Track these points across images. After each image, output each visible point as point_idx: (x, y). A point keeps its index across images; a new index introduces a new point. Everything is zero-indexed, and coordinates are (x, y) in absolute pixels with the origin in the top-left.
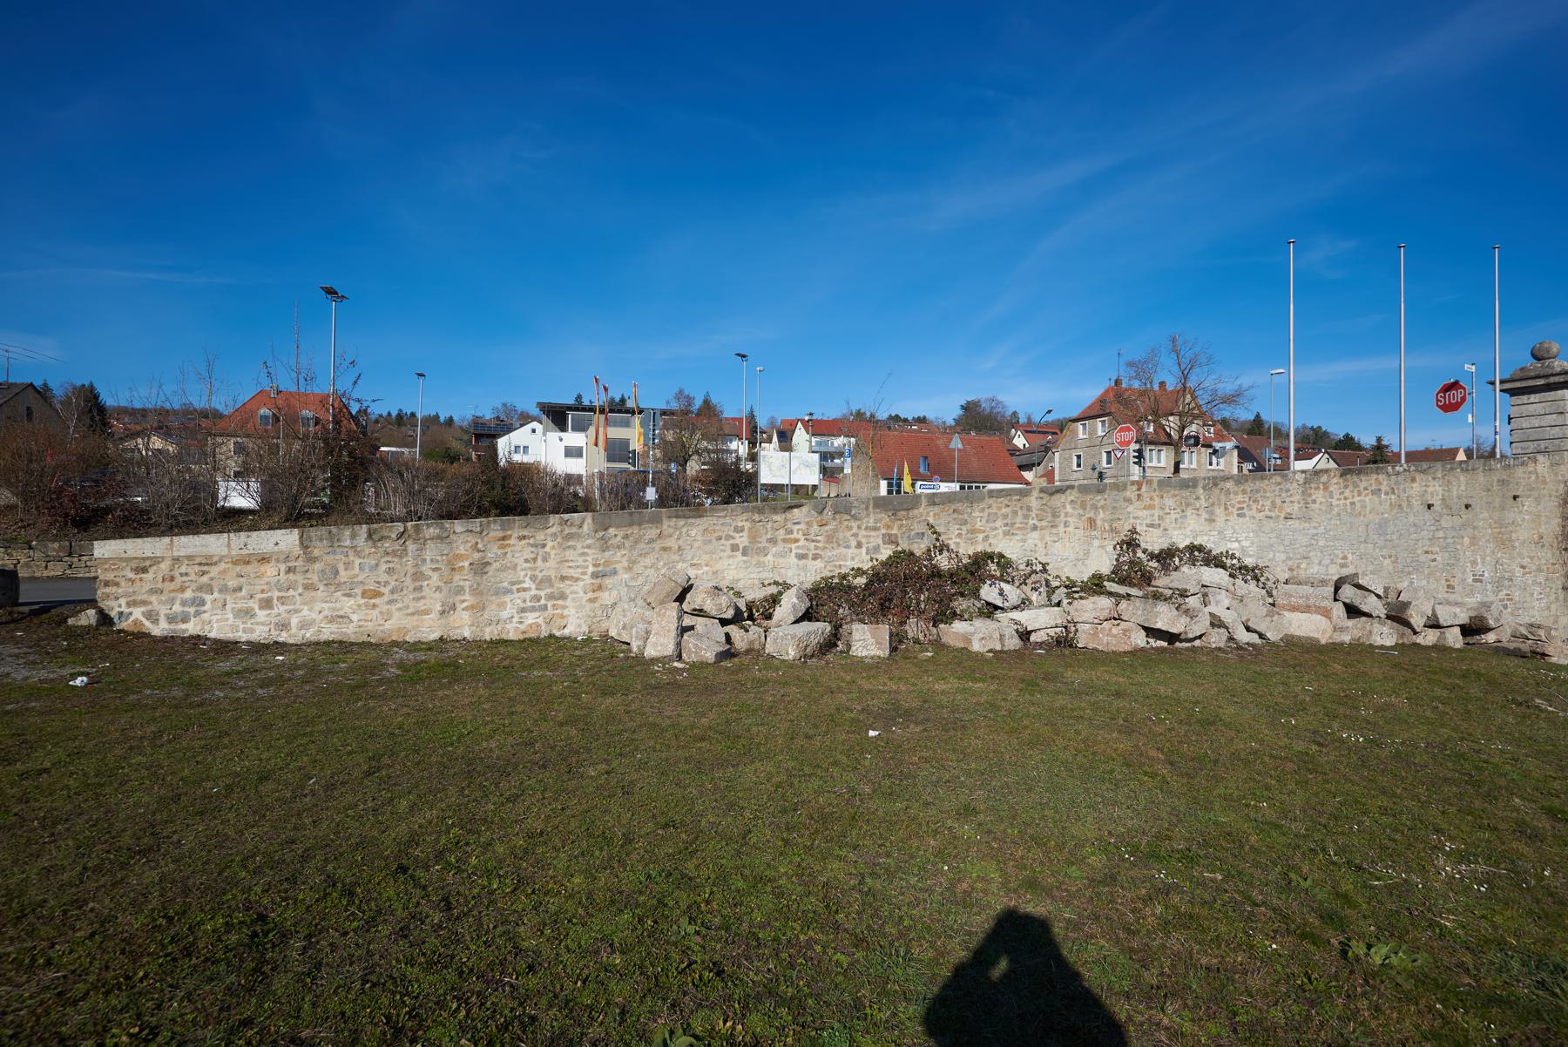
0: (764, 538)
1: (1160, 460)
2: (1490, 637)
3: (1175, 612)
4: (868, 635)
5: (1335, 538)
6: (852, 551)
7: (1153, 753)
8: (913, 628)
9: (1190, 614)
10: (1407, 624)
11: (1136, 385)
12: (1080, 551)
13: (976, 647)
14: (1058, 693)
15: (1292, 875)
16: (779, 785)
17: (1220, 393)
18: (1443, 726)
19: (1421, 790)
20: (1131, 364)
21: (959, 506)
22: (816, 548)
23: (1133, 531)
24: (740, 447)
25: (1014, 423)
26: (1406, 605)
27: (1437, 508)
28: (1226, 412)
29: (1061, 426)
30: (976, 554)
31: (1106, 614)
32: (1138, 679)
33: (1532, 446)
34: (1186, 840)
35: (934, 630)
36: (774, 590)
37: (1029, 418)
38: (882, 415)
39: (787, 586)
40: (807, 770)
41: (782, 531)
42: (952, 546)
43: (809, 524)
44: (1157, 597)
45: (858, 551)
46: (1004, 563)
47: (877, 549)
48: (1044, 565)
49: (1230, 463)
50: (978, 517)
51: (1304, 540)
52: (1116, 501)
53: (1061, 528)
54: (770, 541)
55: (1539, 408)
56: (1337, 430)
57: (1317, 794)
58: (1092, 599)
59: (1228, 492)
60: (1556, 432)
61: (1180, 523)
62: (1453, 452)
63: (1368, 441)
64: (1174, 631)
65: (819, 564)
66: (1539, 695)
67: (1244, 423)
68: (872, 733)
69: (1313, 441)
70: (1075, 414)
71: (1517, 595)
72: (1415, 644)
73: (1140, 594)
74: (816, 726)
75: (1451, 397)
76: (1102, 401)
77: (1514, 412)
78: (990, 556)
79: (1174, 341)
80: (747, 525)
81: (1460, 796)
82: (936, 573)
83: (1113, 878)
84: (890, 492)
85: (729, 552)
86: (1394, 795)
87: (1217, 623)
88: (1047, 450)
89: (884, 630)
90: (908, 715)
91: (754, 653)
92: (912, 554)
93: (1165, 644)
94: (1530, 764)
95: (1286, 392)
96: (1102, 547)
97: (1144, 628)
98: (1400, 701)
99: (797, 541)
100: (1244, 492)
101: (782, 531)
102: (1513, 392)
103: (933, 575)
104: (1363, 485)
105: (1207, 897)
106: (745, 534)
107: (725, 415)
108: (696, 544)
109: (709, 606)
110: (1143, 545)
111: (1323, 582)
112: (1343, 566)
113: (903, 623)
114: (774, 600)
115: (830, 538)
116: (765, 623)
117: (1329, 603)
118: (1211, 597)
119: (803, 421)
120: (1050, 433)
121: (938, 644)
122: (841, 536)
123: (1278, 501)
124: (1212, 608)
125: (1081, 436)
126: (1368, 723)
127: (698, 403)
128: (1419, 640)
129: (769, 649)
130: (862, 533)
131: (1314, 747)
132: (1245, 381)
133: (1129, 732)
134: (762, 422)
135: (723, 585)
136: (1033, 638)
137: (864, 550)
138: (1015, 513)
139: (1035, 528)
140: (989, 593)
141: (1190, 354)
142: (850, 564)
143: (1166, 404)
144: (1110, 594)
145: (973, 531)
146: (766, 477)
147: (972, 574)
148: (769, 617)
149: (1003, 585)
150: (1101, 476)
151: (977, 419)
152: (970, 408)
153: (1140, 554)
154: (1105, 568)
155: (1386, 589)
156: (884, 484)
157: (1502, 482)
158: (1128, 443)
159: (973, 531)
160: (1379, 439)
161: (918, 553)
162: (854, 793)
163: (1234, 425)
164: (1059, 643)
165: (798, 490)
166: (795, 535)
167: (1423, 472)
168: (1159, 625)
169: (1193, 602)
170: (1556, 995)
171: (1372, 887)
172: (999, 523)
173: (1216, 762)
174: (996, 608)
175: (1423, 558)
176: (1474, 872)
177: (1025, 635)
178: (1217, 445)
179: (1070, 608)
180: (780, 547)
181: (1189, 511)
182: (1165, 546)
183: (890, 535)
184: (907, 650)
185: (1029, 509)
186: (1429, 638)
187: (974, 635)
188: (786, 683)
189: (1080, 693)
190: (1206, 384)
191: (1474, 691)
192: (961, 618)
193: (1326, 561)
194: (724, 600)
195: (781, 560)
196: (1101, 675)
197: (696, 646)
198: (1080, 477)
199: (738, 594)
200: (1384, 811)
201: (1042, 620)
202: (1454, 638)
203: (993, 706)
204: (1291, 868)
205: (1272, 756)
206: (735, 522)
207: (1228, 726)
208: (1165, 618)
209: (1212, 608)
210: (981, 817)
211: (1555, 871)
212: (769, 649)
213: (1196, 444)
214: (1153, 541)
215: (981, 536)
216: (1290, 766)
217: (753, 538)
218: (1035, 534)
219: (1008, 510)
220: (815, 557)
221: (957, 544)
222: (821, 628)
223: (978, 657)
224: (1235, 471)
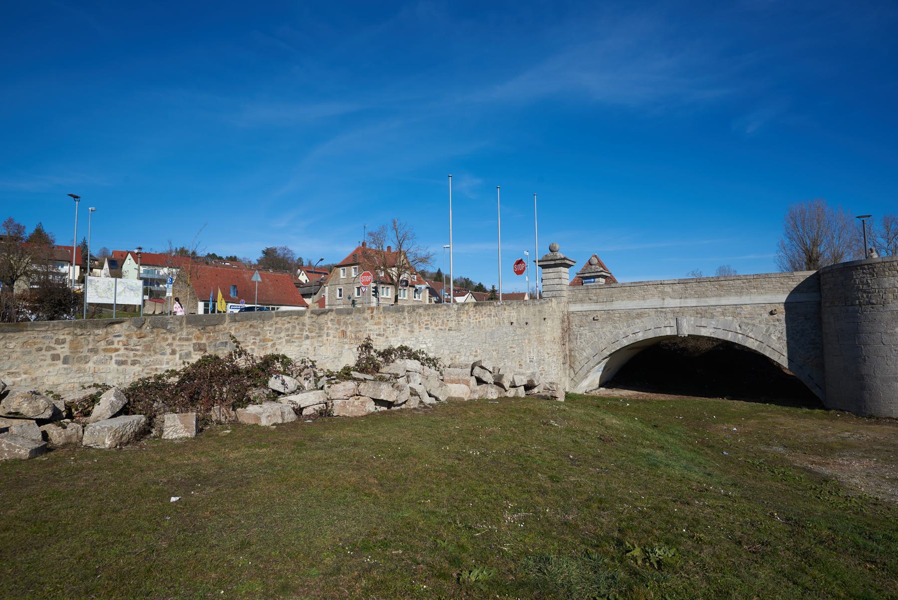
0: (86, 349)
1: (387, 293)
2: (535, 390)
3: (391, 388)
4: (178, 422)
5: (472, 341)
6: (168, 357)
7: (372, 481)
8: (216, 413)
9: (399, 389)
10: (502, 386)
11: (374, 247)
12: (335, 352)
13: (264, 422)
14: (318, 448)
15: (438, 541)
16: (83, 556)
17: (419, 256)
18: (514, 440)
19: (502, 477)
20: (371, 234)
21: (254, 322)
22: (135, 355)
23: (369, 339)
24: (72, 272)
25: (299, 265)
26: (501, 376)
27: (514, 324)
28: (420, 267)
29: (330, 270)
30: (266, 357)
31: (351, 392)
32: (368, 433)
33: (550, 294)
34: (385, 533)
35: (233, 413)
36: (93, 391)
37: (310, 263)
38: (202, 253)
39: (106, 388)
40: (110, 539)
41: (103, 343)
42: (249, 351)
43: (129, 337)
44: (382, 379)
45: (172, 357)
46: (286, 361)
47: (188, 355)
48: (313, 362)
49: (424, 297)
50: (268, 330)
51: (457, 342)
52: (359, 320)
53: (325, 337)
54: (91, 350)
55: (552, 275)
56: (476, 281)
57: (455, 489)
58: (343, 383)
59: (420, 315)
60: (558, 287)
61: (395, 333)
62: (523, 295)
63: (489, 287)
64: (391, 400)
65: (137, 368)
66: (552, 418)
67: (432, 274)
68: (173, 499)
69: (464, 286)
70: (338, 262)
71: (546, 368)
72: (506, 397)
73: (372, 378)
74: (124, 501)
75: (519, 267)
76: (354, 255)
77: (544, 276)
78: (276, 358)
79: (394, 222)
80: (69, 338)
81: (517, 477)
82: (236, 371)
83: (339, 569)
84: (206, 311)
85: (49, 361)
86: (490, 482)
87: (414, 393)
88: (321, 284)
89: (192, 417)
90: (206, 480)
91: (72, 446)
92: (217, 358)
93: (385, 409)
94: (547, 455)
95: (451, 257)
96: (350, 349)
97: (374, 400)
98: (497, 429)
99: (117, 350)
100: (429, 315)
101: (103, 343)
102: (543, 267)
103: (234, 373)
104: (484, 312)
105: (393, 566)
106: (66, 345)
107: (58, 243)
108: (14, 355)
109: (25, 408)
110: (374, 347)
111: (466, 366)
112: (476, 356)
113: (209, 410)
114: (94, 400)
115: (147, 348)
116: (84, 420)
117: (468, 377)
118: (411, 378)
119: (133, 254)
120: (322, 274)
121: (236, 424)
122: (157, 345)
123: (445, 320)
124: (411, 385)
125: (342, 277)
126: (482, 443)
127: (29, 231)
128: (508, 394)
129: (86, 441)
130: (177, 342)
131: (457, 462)
132: (432, 250)
133: (358, 469)
134: (94, 250)
135: (42, 389)
136: (304, 413)
137: (177, 356)
138: (294, 327)
139: (307, 337)
140: (274, 383)
141: (403, 232)
142: (165, 367)
143: (391, 260)
144: (355, 379)
145: (264, 340)
146: (92, 297)
147: (263, 370)
148: (88, 414)
149: (285, 377)
150: (354, 303)
151: (273, 261)
152: (268, 253)
153: (372, 353)
154: (352, 363)
155: (494, 368)
156: (201, 305)
157: (540, 311)
158: (369, 283)
159: (264, 340)
160: (493, 287)
161: (222, 357)
162: (152, 549)
163: (428, 275)
164: (321, 414)
165: (126, 308)
166: (116, 346)
167: (509, 305)
168: (382, 397)
169: (401, 381)
170: (544, 574)
171: (475, 537)
172: (283, 334)
173: (406, 479)
174: (280, 393)
175: (509, 351)
176: (519, 517)
177: (299, 411)
178: (418, 286)
179: (329, 390)
180: (101, 356)
181: (400, 326)
182: (387, 348)
183: (199, 344)
184: (211, 430)
185: (304, 325)
186: (511, 393)
187: (263, 414)
188: (100, 469)
189: (332, 447)
190: (411, 250)
191: (528, 420)
192: (254, 402)
193: (468, 354)
194: (41, 403)
195: (101, 367)
196: (348, 433)
197: (9, 446)
198: (341, 304)
199: (58, 397)
200: (485, 492)
201: (310, 400)
202: (521, 392)
203: (272, 464)
204: (438, 537)
205: (435, 471)
206: (60, 336)
207: (414, 456)
208: (386, 392)
209: (411, 385)
210: (253, 548)
211: (551, 508)
212: (86, 441)
213: (406, 286)
214: (380, 345)
215: (270, 344)
216: (444, 475)
217: (75, 349)
218: (308, 342)
219: (289, 325)
220: (134, 363)
221: (253, 350)
222: (136, 420)
223: (266, 430)
224: (427, 303)
